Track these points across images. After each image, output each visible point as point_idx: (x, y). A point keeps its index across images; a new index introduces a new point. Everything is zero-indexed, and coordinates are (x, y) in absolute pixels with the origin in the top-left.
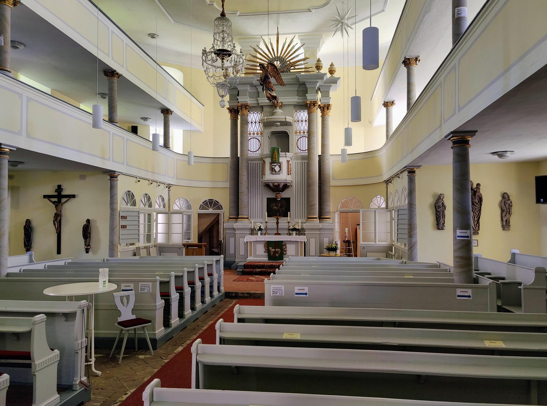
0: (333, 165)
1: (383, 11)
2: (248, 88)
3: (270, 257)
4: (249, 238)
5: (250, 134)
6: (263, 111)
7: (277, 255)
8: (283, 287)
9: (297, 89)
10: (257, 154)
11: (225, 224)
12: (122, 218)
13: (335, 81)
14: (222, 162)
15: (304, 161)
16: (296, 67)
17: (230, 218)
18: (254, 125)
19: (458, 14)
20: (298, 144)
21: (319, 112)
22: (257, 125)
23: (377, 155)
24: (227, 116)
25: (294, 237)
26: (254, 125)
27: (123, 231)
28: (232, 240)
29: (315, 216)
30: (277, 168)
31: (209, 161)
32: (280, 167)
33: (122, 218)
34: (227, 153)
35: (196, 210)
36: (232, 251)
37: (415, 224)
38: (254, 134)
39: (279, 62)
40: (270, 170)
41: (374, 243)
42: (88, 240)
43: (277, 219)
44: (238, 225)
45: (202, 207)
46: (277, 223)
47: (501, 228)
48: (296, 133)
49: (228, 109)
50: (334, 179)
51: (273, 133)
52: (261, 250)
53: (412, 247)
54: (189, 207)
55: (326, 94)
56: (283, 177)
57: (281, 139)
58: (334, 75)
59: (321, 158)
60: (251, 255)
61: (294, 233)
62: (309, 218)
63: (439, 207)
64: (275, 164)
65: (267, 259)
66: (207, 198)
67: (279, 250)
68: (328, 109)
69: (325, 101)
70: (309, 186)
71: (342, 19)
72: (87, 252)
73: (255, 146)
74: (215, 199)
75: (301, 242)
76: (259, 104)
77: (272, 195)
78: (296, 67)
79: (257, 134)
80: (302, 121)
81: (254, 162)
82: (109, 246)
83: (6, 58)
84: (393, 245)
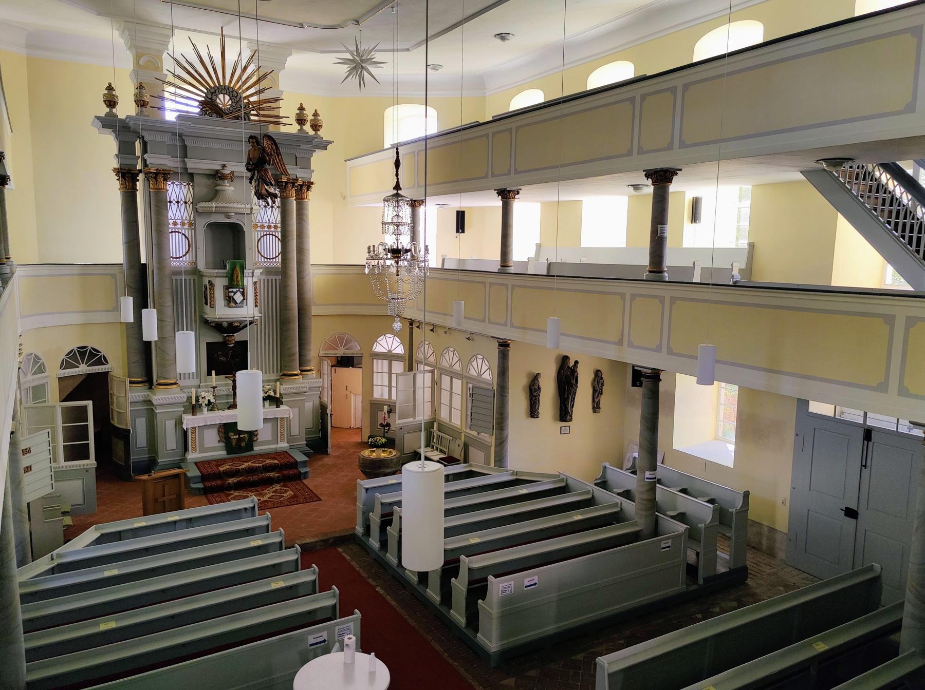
3: (230, 448)
4: (189, 421)
6: (192, 180)
7: (243, 444)
10: (185, 263)
11: (127, 398)
13: (324, 146)
14: (102, 272)
15: (270, 277)
16: (262, 112)
20: (262, 250)
21: (293, 193)
29: (295, 372)
30: (238, 297)
31: (75, 272)
32: (243, 294)
34: (117, 254)
35: (54, 372)
36: (140, 438)
39: (227, 98)
40: (225, 299)
41: (412, 419)
45: (65, 365)
47: (591, 410)
48: (256, 226)
51: (213, 227)
53: (501, 443)
55: (307, 166)
56: (248, 310)
57: (229, 239)
58: (319, 133)
60: (194, 450)
62: (284, 375)
64: (235, 290)
66: (74, 345)
68: (308, 188)
70: (284, 323)
73: (180, 250)
74: (91, 344)
75: (282, 419)
76: (186, 169)
77: (216, 338)
78: (262, 112)
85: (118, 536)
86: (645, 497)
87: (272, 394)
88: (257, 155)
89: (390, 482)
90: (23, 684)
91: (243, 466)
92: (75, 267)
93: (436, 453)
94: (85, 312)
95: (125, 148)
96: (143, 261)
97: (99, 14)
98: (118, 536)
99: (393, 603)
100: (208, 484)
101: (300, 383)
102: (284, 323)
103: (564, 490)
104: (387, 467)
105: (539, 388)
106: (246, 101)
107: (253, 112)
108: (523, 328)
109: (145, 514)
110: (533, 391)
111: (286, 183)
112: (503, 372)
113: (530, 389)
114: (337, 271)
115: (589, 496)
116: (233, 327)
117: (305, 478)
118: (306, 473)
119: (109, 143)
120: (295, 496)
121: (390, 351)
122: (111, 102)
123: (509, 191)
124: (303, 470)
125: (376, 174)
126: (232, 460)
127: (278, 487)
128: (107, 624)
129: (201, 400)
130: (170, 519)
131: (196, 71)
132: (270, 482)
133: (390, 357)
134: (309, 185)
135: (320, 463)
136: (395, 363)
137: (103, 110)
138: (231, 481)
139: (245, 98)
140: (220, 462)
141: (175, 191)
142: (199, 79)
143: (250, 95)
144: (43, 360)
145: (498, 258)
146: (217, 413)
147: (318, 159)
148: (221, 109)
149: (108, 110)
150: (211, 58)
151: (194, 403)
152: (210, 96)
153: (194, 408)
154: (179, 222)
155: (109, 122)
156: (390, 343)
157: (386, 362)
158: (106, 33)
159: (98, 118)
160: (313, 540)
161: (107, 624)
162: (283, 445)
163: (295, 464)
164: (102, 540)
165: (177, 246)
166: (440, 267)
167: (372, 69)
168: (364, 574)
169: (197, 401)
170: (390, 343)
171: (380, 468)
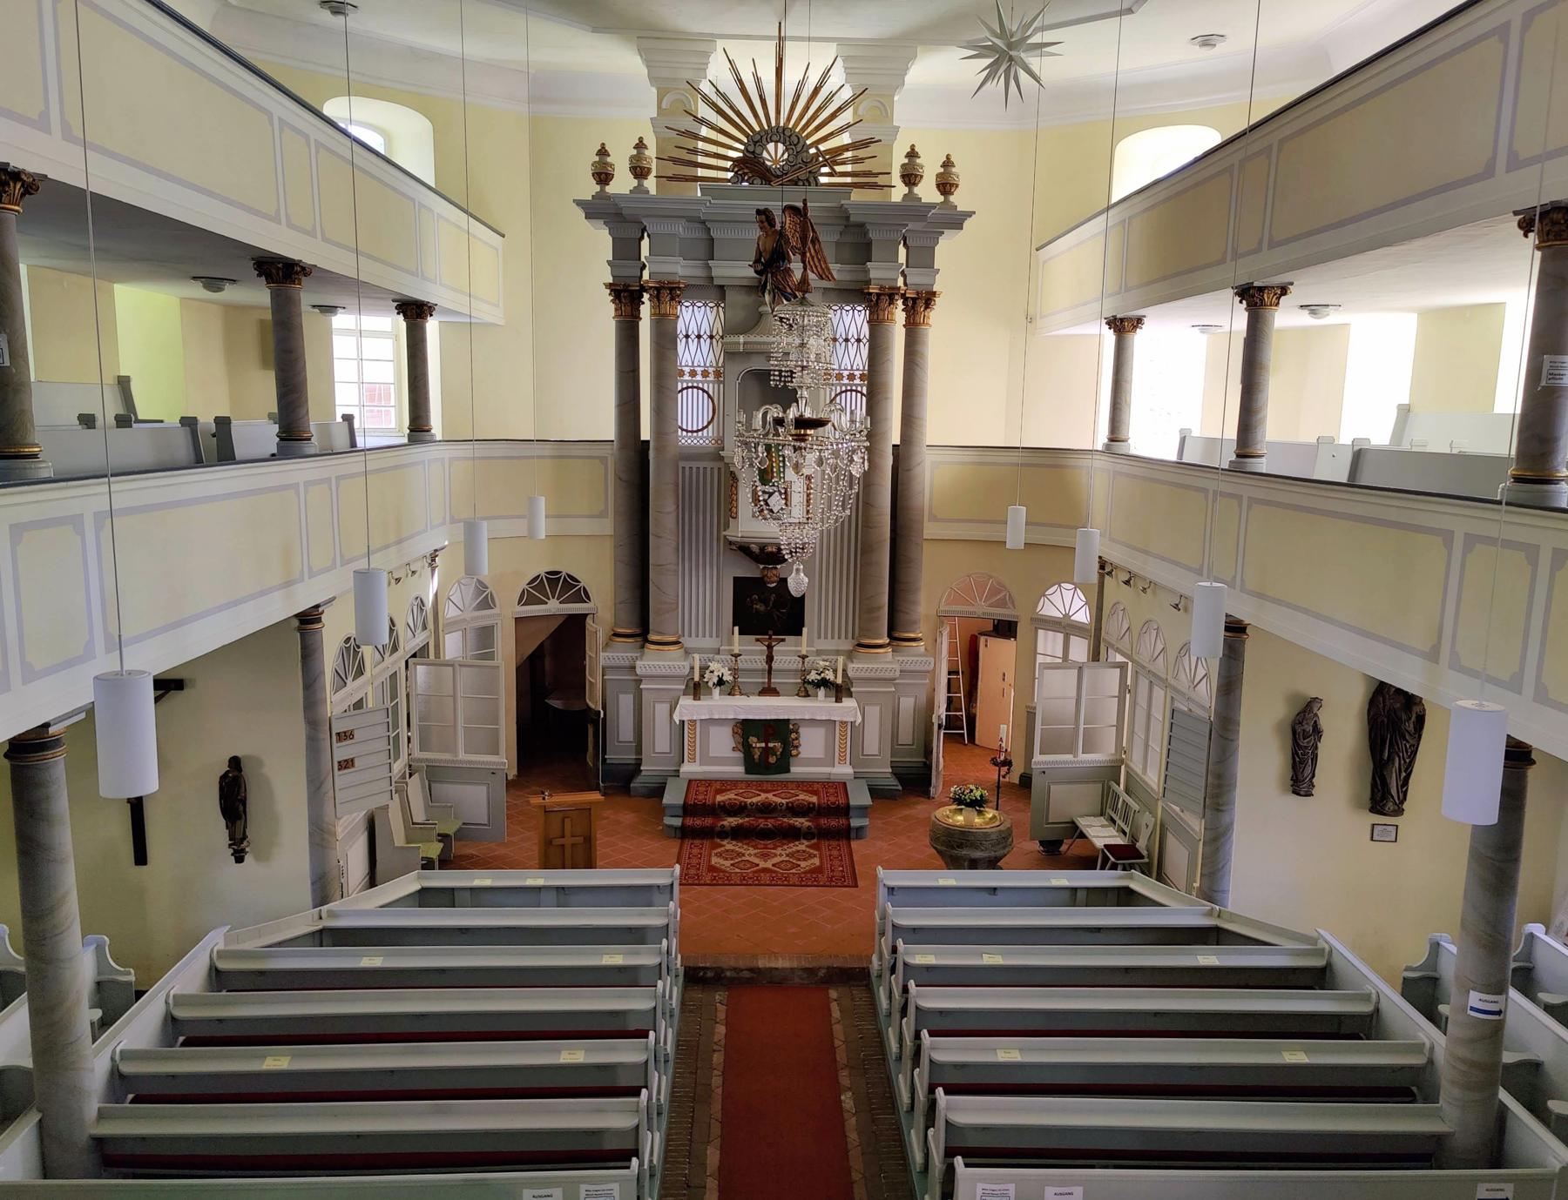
0: (933, 476)
1: (1130, 11)
2: (680, 229)
3: (751, 765)
4: (688, 708)
5: (682, 373)
6: (723, 299)
7: (772, 760)
8: (1012, 1187)
9: (836, 237)
10: (705, 440)
11: (605, 656)
12: (339, 740)
13: (956, 221)
14: (586, 453)
16: (838, 169)
17: (617, 635)
18: (693, 345)
19: (1553, 376)
21: (899, 315)
22: (705, 345)
23: (1071, 462)
24: (606, 309)
25: (822, 705)
26: (693, 345)
27: (343, 778)
28: (626, 702)
29: (880, 642)
30: (776, 502)
31: (547, 453)
33: (339, 740)
34: (606, 427)
35: (508, 609)
36: (623, 728)
37: (1233, 776)
38: (693, 373)
39: (781, 147)
42: (239, 824)
43: (770, 647)
44: (652, 662)
45: (527, 598)
46: (770, 659)
49: (609, 286)
50: (933, 518)
52: (723, 744)
53: (1217, 839)
54: (486, 603)
55: (923, 258)
58: (952, 198)
59: (902, 456)
60: (693, 760)
61: (822, 692)
62: (860, 645)
63: (1306, 736)
65: (741, 769)
66: (541, 569)
67: (778, 745)
69: (916, 277)
70: (865, 549)
71: (1010, 46)
72: (239, 860)
74: (565, 568)
77: (749, 570)
78: (838, 169)
79: (705, 374)
80: (847, 340)
81: (694, 464)
82: (311, 835)
83: (23, 411)
84: (1122, 761)
85: (448, 897)
86: (1463, 1052)
87: (829, 675)
88: (770, 244)
89: (942, 883)
90: (85, 1138)
91: (755, 800)
92: (548, 446)
93: (1112, 831)
94: (559, 516)
95: (625, 250)
96: (645, 435)
97: (595, 30)
98: (448, 897)
99: (853, 1136)
100: (690, 821)
101: (886, 662)
102: (865, 549)
103: (1320, 977)
104: (977, 848)
105: (1317, 732)
106: (813, 151)
107: (825, 170)
108: (1260, 596)
109: (546, 865)
110: (1303, 736)
111: (878, 295)
112: (1229, 686)
113: (1294, 732)
114: (976, 459)
115: (1366, 1008)
116: (770, 556)
117: (858, 838)
118: (861, 828)
119: (601, 241)
120: (818, 870)
121: (1067, 616)
122: (603, 176)
123: (1261, 289)
124: (855, 823)
125: (1081, 265)
126: (748, 784)
127: (802, 845)
128: (278, 1061)
129: (707, 675)
130: (530, 882)
131: (732, 107)
132: (793, 834)
133: (1066, 627)
134: (928, 298)
135: (907, 812)
136: (1074, 640)
137: (590, 189)
138: (731, 822)
139: (811, 145)
140: (726, 784)
141: (695, 317)
142: (736, 119)
143: (822, 141)
144: (523, 585)
145: (1232, 433)
146: (739, 701)
147: (947, 249)
148: (768, 169)
149: (598, 188)
150: (758, 81)
151: (697, 678)
152: (751, 149)
153: (697, 689)
154: (699, 370)
155: (599, 209)
156: (1068, 602)
157: (1060, 636)
158: (619, 61)
159: (579, 203)
160: (787, 964)
161: (278, 1061)
162: (843, 770)
163: (845, 810)
164: (425, 897)
165: (692, 411)
166: (1174, 458)
167: (1034, 62)
168: (841, 1056)
169: (702, 676)
170: (1068, 602)
171: (960, 846)
